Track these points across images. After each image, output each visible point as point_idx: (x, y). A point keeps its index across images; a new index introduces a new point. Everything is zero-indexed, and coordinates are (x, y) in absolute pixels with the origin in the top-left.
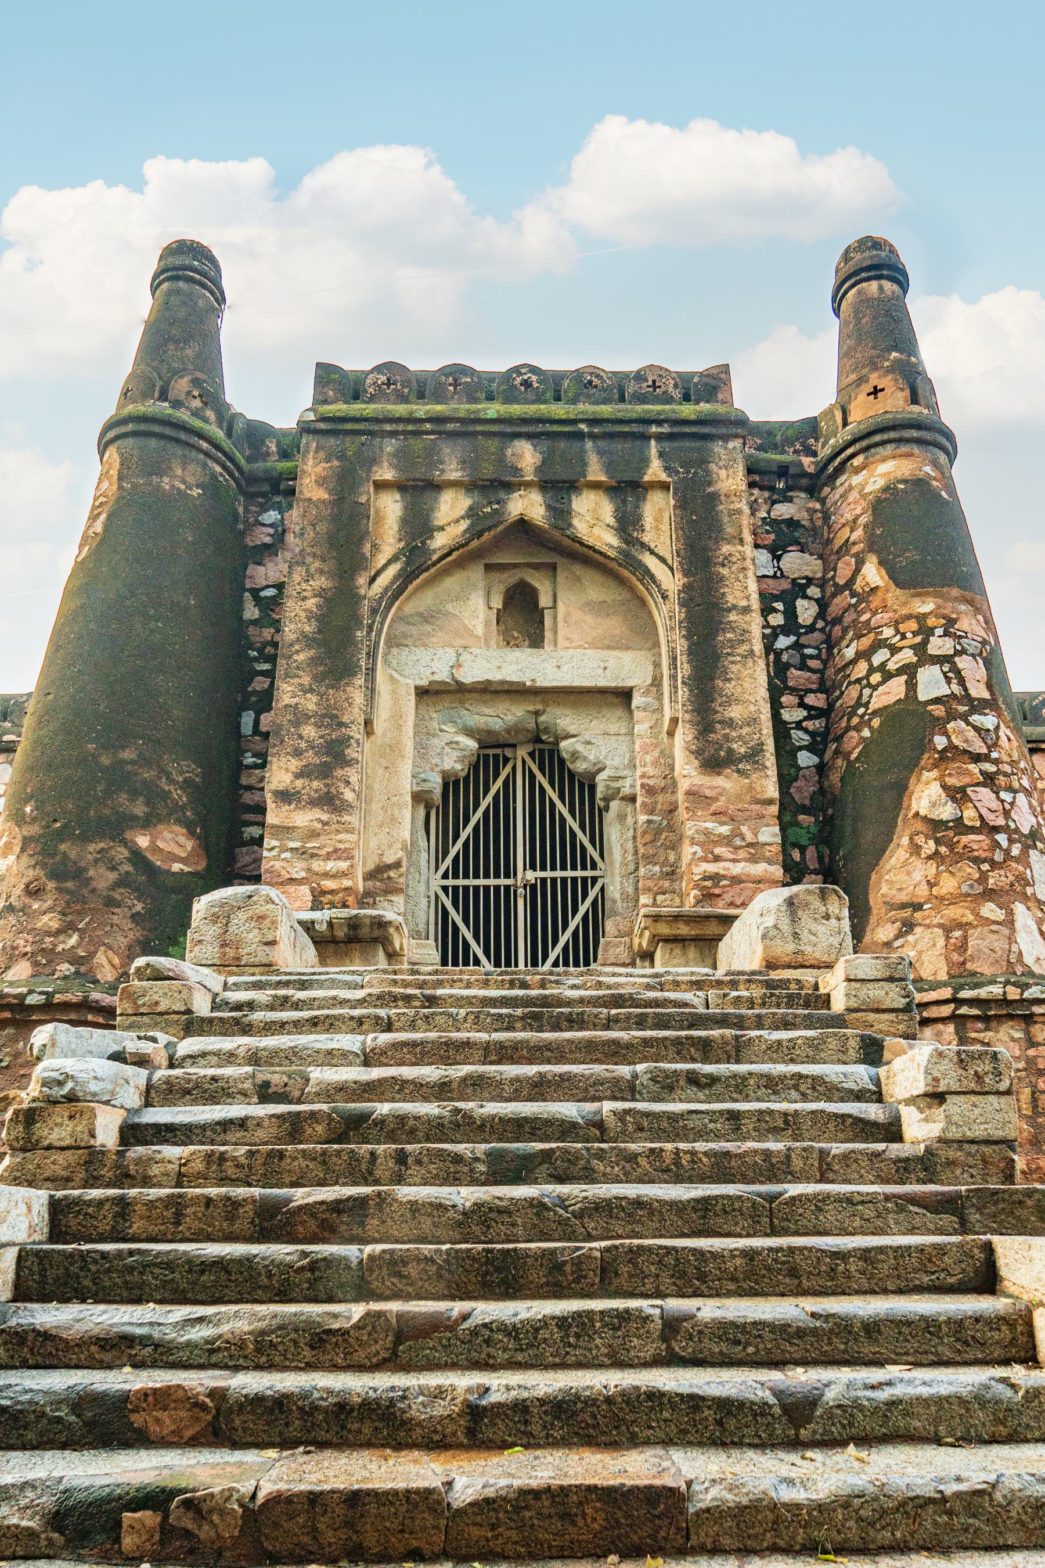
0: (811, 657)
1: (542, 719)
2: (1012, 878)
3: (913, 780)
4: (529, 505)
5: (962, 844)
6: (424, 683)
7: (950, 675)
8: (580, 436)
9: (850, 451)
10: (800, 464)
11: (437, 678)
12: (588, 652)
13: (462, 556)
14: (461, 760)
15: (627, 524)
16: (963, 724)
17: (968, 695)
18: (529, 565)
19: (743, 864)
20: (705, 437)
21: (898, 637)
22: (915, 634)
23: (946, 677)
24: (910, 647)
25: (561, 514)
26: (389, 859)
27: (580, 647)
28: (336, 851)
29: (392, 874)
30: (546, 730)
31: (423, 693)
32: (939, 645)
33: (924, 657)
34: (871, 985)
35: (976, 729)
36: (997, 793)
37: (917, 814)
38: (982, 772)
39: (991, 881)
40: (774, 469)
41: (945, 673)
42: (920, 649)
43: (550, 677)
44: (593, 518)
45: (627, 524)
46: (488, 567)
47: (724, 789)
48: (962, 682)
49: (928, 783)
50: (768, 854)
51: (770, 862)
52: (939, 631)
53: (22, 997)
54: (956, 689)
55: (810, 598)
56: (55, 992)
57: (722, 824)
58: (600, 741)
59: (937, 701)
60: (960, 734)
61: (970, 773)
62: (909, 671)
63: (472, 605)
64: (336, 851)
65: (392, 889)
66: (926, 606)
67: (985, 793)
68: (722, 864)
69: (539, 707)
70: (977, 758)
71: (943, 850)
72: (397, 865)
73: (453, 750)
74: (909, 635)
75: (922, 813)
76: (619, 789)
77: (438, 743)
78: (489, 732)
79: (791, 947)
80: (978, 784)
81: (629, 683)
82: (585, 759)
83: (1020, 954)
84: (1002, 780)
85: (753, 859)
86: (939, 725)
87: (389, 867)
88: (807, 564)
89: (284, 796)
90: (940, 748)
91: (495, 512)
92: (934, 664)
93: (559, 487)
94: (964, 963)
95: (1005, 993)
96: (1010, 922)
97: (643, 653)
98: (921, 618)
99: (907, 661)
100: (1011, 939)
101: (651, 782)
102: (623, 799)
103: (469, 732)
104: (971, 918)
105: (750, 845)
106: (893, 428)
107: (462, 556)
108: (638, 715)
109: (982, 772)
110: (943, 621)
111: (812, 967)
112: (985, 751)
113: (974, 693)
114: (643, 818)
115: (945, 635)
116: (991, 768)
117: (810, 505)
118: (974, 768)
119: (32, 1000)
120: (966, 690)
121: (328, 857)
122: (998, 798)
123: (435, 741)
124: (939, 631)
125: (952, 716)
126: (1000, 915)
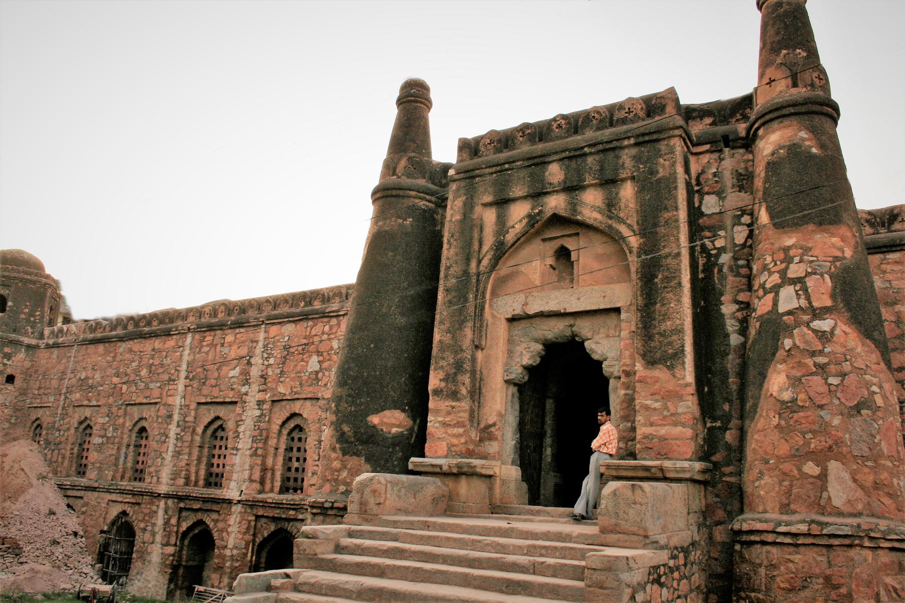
0: (742, 267)
1: (574, 329)
2: (830, 442)
3: (770, 370)
4: (556, 203)
5: (794, 419)
6: (509, 316)
7: (800, 292)
8: (585, 155)
9: (756, 126)
10: (736, 132)
11: (516, 312)
12: (596, 287)
13: (526, 237)
14: (532, 357)
15: (611, 204)
16: (805, 329)
17: (812, 306)
18: (563, 236)
19: (667, 427)
20: (657, 140)
21: (773, 264)
22: (782, 262)
23: (797, 294)
24: (778, 272)
25: (573, 206)
26: (491, 422)
27: (591, 285)
28: (458, 422)
29: (492, 429)
30: (577, 335)
31: (512, 320)
32: (796, 270)
33: (786, 281)
34: (598, 572)
35: (815, 331)
36: (826, 379)
37: (772, 395)
38: (815, 364)
39: (812, 446)
40: (719, 137)
41: (796, 291)
42: (783, 273)
43: (574, 306)
44: (591, 204)
45: (611, 204)
46: (544, 240)
47: (659, 378)
48: (808, 298)
49: (779, 373)
50: (683, 420)
51: (684, 425)
52: (797, 259)
53: (323, 503)
54: (803, 303)
55: (743, 224)
56: (335, 502)
57: (657, 401)
58: (604, 342)
59: (790, 313)
60: (800, 337)
61: (806, 365)
62: (776, 289)
63: (535, 263)
64: (458, 422)
65: (491, 438)
66: (790, 241)
67: (817, 380)
68: (654, 428)
69: (572, 322)
70: (813, 354)
71: (783, 423)
72: (494, 425)
73: (528, 353)
74: (778, 263)
75: (774, 394)
76: (612, 373)
77: (519, 349)
78: (546, 340)
79: (613, 521)
80: (812, 374)
81: (618, 305)
82: (596, 353)
83: (829, 498)
84: (832, 368)
85: (675, 424)
86: (788, 330)
87: (491, 426)
88: (743, 200)
89: (437, 392)
90: (787, 348)
91: (541, 211)
92: (790, 284)
93: (572, 188)
94: (788, 505)
95: (809, 529)
96: (823, 477)
97: (623, 284)
98: (786, 250)
99: (776, 282)
100: (824, 488)
101: (628, 369)
102: (615, 378)
103: (536, 341)
104: (796, 472)
105: (672, 415)
106: (777, 109)
107: (526, 237)
108: (623, 325)
109: (815, 364)
110: (800, 251)
111: (624, 533)
112: (820, 348)
113: (816, 304)
114: (623, 392)
115: (800, 262)
116: (821, 360)
117: (745, 157)
118: (809, 362)
119: (327, 505)
120: (810, 303)
121: (455, 426)
122: (826, 383)
123: (518, 348)
124: (797, 259)
125: (797, 324)
126: (816, 471)
